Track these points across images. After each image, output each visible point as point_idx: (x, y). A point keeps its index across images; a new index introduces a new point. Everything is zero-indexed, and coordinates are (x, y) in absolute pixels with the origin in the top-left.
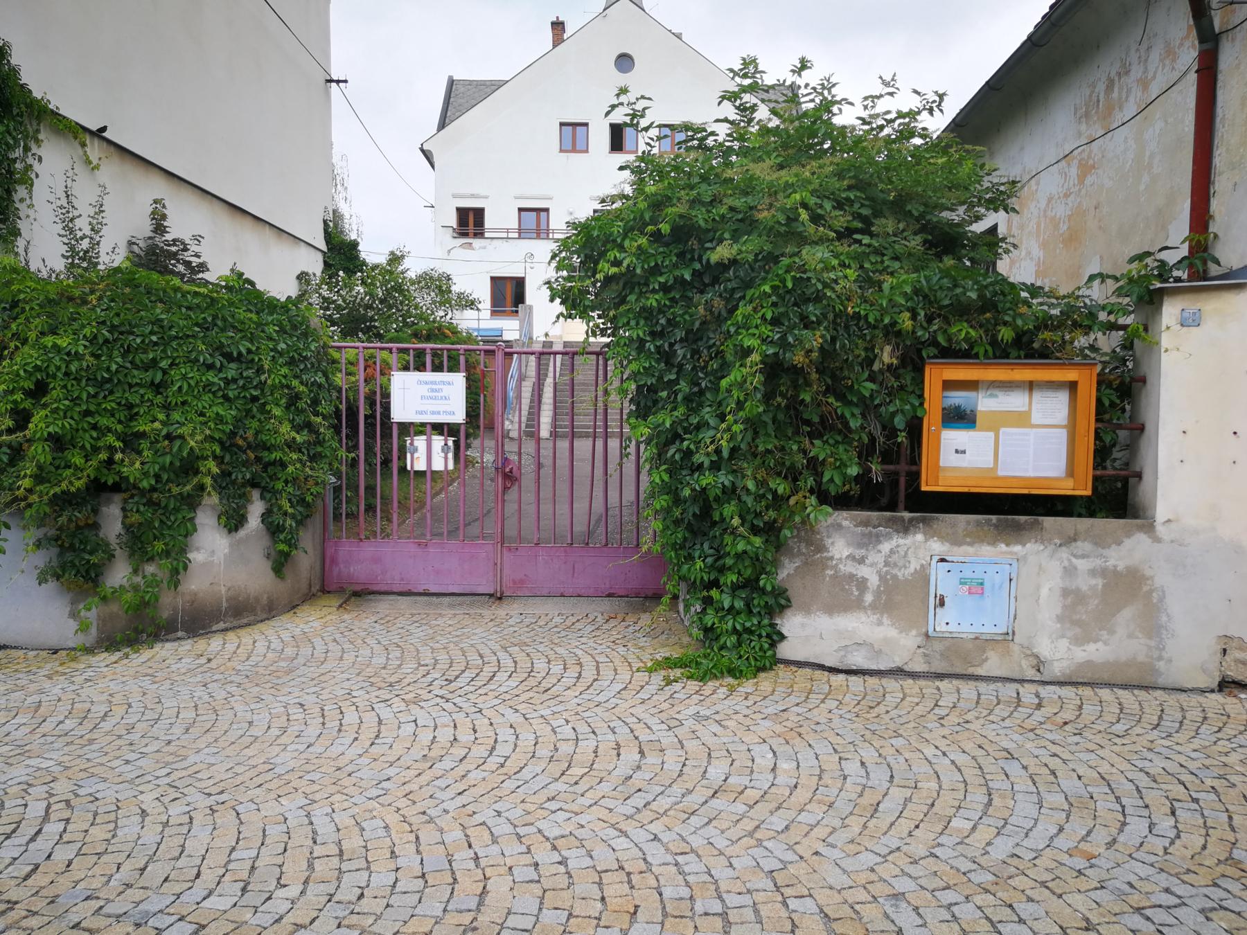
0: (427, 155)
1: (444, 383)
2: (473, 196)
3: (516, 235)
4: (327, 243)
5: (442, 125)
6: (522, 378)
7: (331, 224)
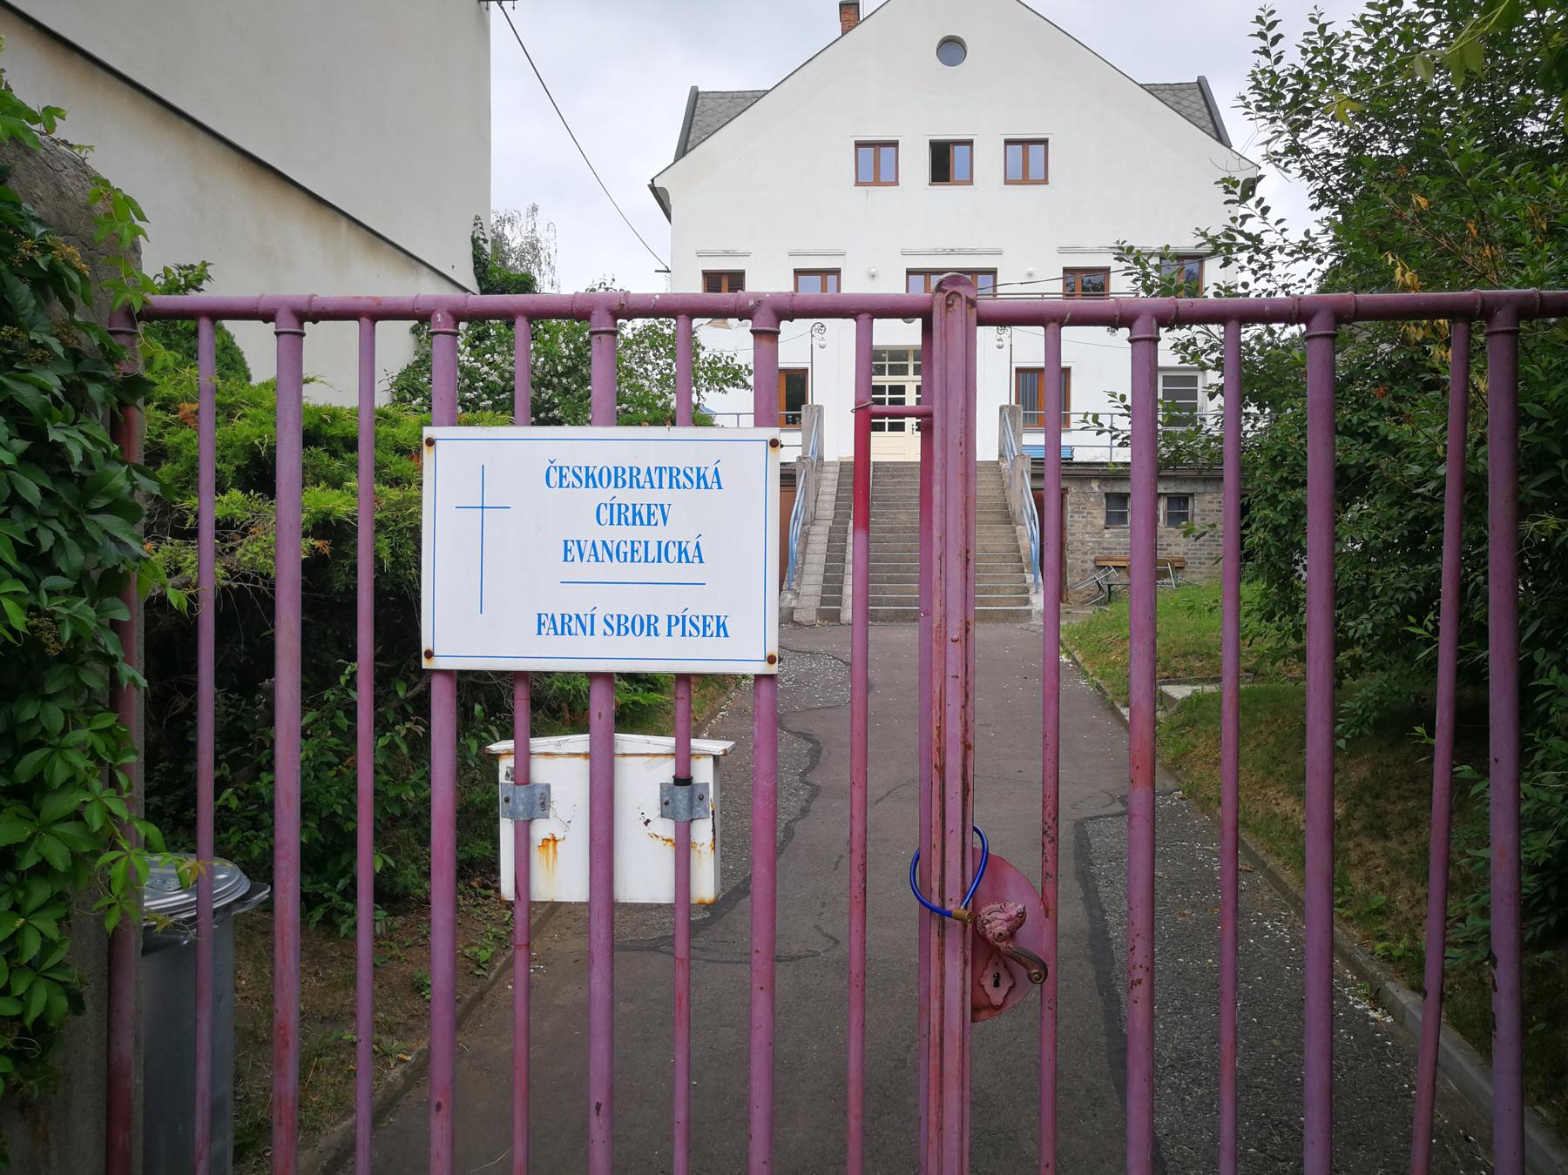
1: (673, 477)
5: (683, 150)
6: (814, 520)
7: (488, 248)
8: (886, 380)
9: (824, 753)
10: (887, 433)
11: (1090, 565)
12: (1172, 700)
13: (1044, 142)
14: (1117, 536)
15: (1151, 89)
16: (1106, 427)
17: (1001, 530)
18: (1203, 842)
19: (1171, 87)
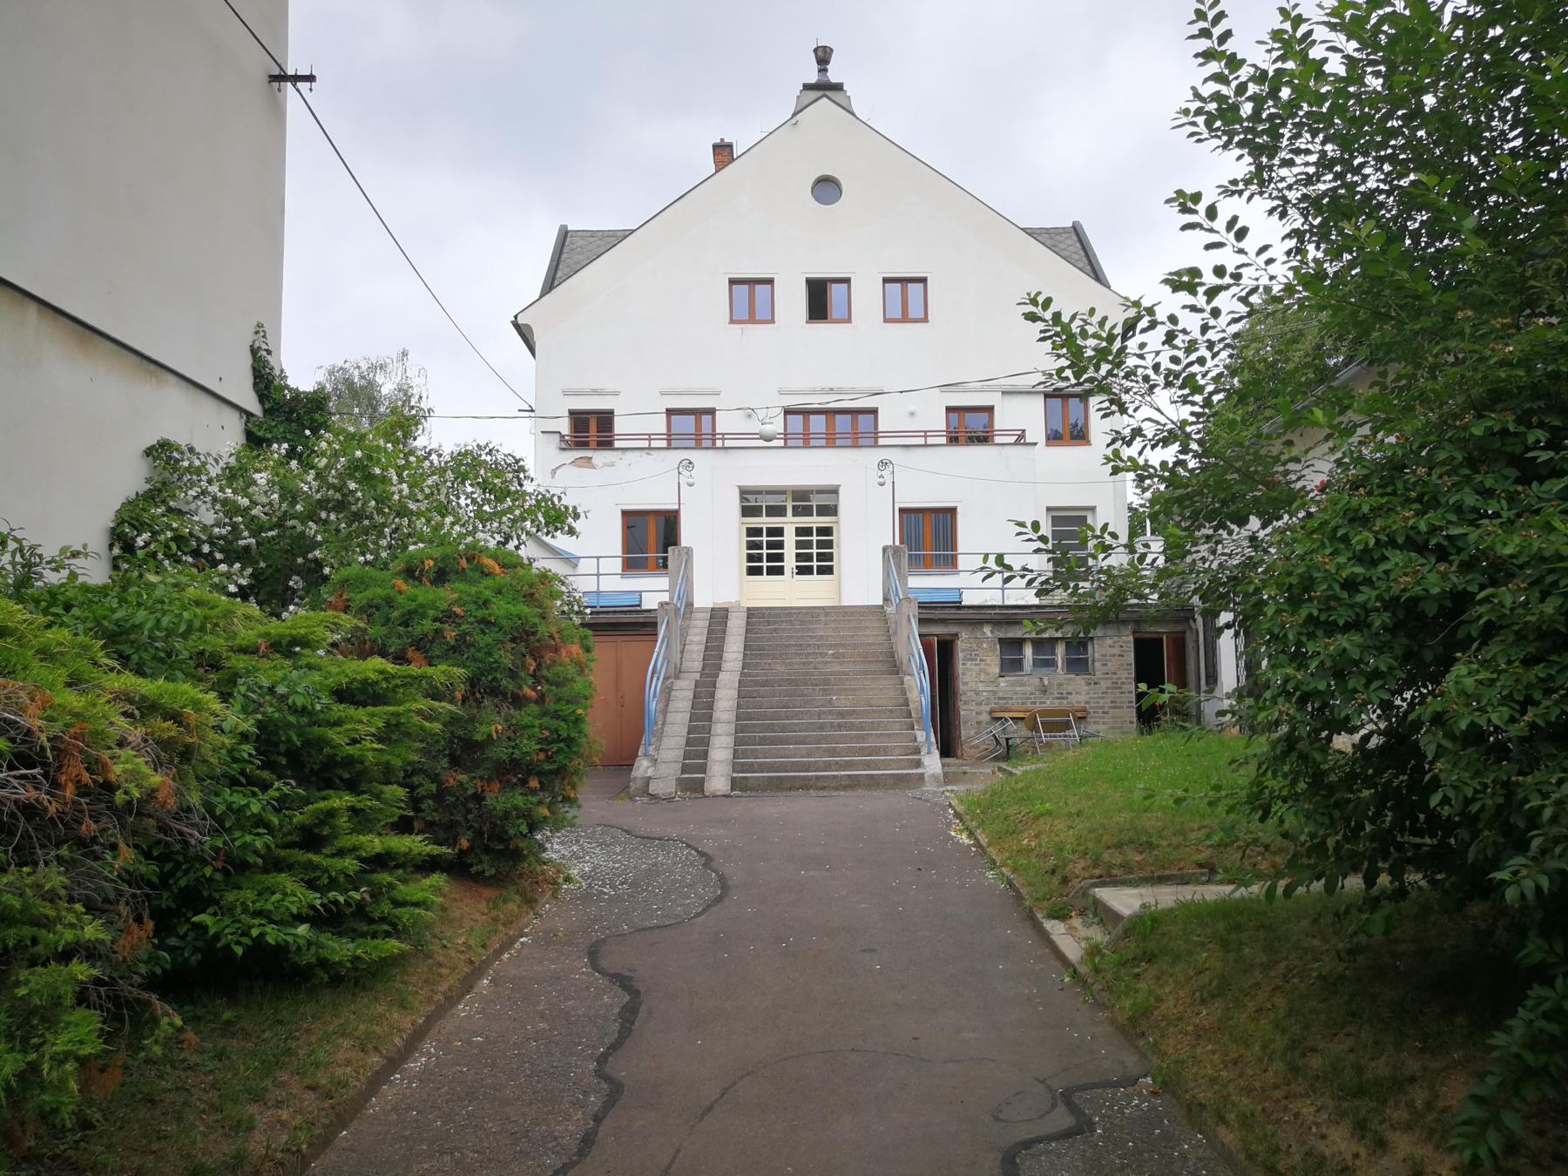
2: (595, 392)
3: (664, 444)
4: (262, 397)
5: (550, 285)
6: (678, 673)
8: (764, 522)
9: (642, 1014)
10: (765, 577)
11: (985, 717)
12: (1116, 917)
13: (923, 280)
17: (887, 681)
19: (1047, 231)
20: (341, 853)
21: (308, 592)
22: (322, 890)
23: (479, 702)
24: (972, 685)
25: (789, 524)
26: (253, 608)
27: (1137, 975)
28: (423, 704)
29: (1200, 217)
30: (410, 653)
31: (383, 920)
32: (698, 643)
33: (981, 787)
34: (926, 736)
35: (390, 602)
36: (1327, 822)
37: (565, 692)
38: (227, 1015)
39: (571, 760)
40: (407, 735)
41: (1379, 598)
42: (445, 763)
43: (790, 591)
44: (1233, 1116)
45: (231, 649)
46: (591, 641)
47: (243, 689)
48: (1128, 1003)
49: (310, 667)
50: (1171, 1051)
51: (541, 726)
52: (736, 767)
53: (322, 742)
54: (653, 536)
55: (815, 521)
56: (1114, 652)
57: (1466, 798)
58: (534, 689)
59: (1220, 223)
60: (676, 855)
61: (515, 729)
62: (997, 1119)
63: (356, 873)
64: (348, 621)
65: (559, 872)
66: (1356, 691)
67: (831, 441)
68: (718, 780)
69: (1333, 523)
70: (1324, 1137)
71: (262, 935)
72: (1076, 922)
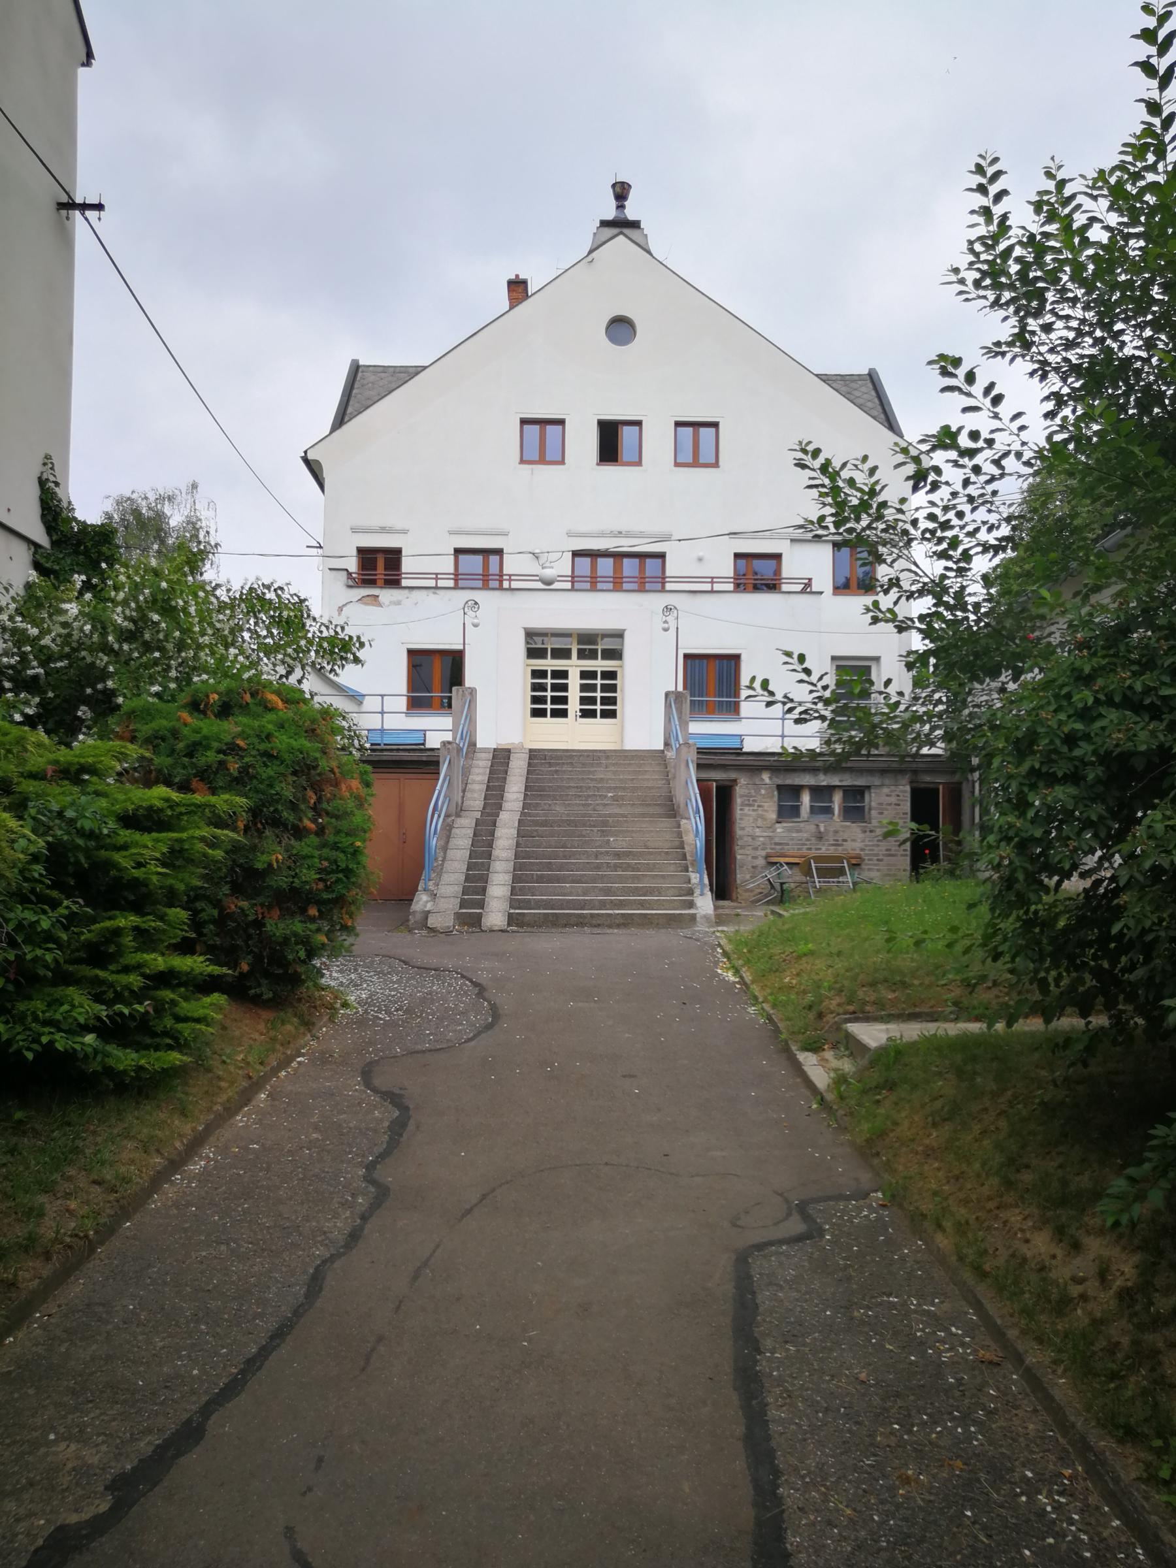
0: (314, 468)
2: (383, 530)
3: (451, 583)
5: (340, 420)
6: (460, 811)
8: (549, 664)
9: (411, 1126)
11: (761, 862)
12: (863, 1048)
13: (715, 425)
14: (790, 830)
15: (825, 378)
16: (779, 697)
17: (665, 824)
18: (921, 1297)
19: (843, 378)
20: (126, 970)
21: (95, 723)
22: (109, 1004)
23: (260, 833)
24: (749, 830)
25: (574, 667)
26: (41, 735)
27: (878, 1101)
28: (206, 831)
29: (959, 382)
30: (195, 783)
31: (166, 1034)
32: (481, 783)
33: (749, 928)
34: (699, 878)
35: (175, 734)
36: (1037, 957)
37: (344, 825)
38: (19, 1115)
39: (349, 890)
40: (190, 861)
41: (1094, 752)
42: (226, 889)
43: (573, 733)
44: (949, 1224)
45: (22, 775)
46: (371, 777)
47: (33, 812)
48: (866, 1126)
49: (97, 793)
50: (901, 1168)
51: (321, 858)
52: (513, 904)
53: (109, 864)
54: (437, 675)
55: (599, 665)
56: (891, 802)
57: (1143, 928)
58: (314, 821)
59: (978, 389)
60: (450, 985)
61: (296, 859)
62: (735, 1225)
63: (141, 989)
64: (134, 750)
65: (336, 997)
66: (1069, 838)
67: (618, 584)
68: (495, 915)
69: (1060, 682)
70: (1027, 1241)
71: (51, 1043)
72: (829, 1054)
